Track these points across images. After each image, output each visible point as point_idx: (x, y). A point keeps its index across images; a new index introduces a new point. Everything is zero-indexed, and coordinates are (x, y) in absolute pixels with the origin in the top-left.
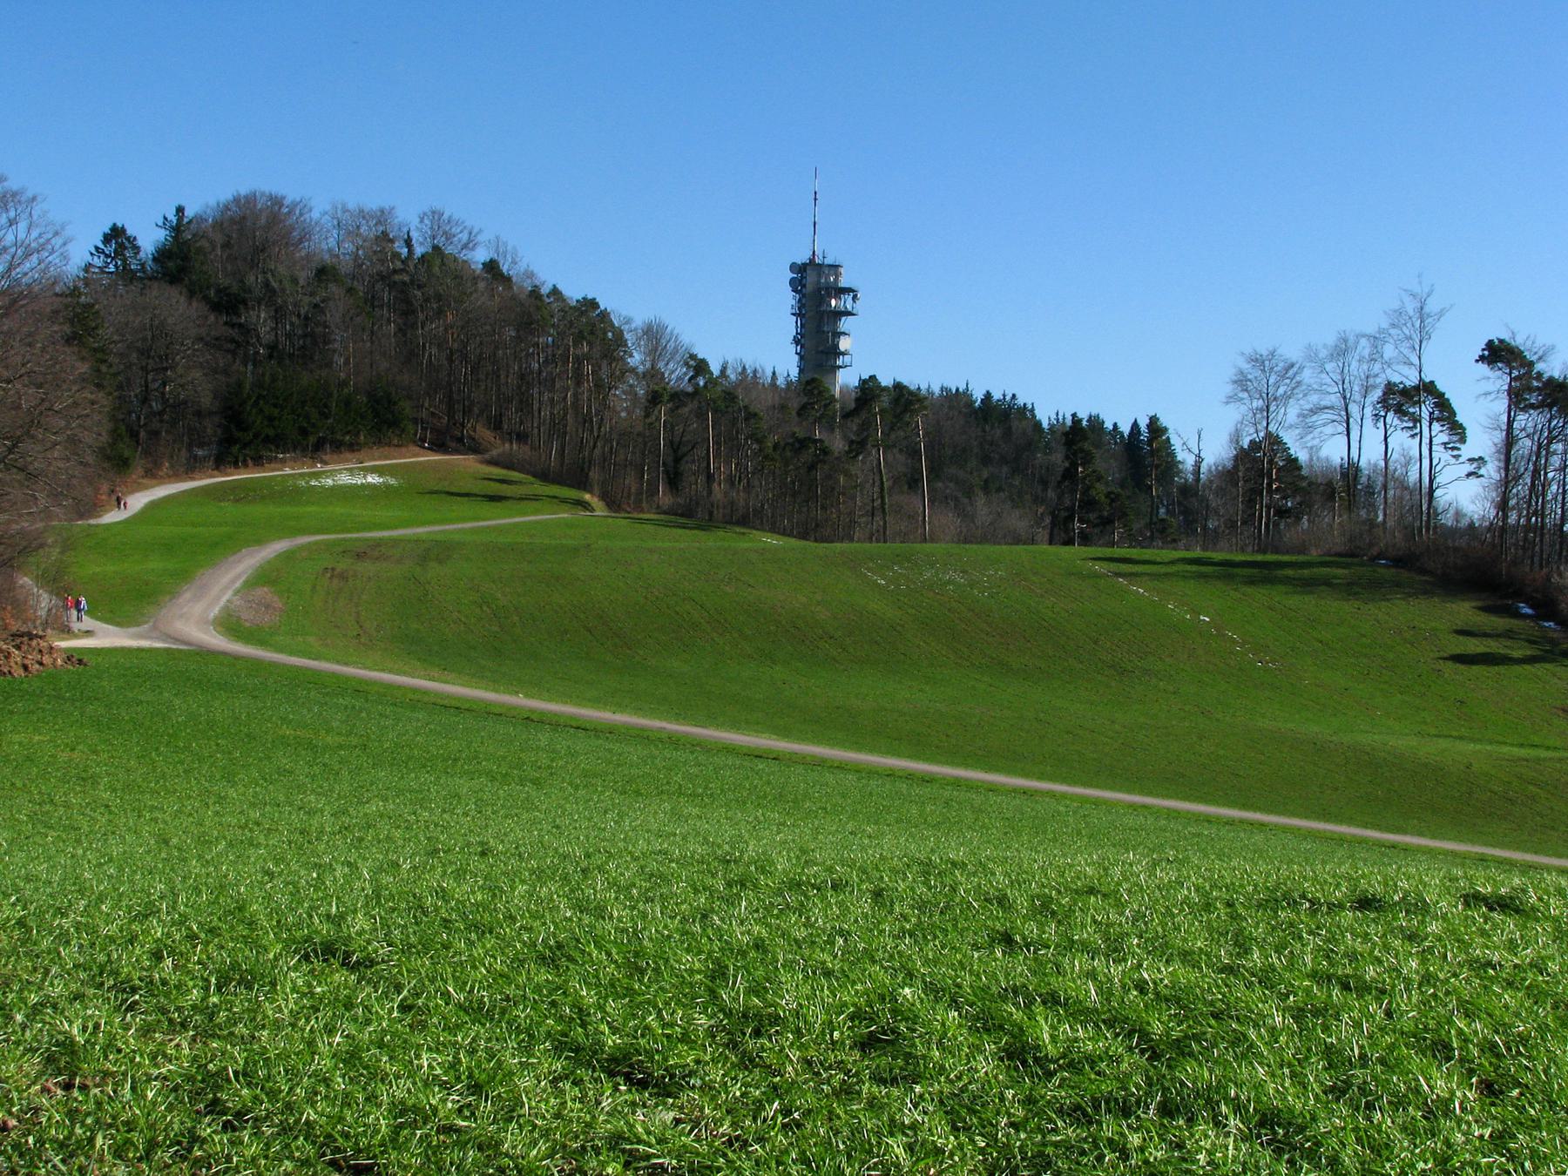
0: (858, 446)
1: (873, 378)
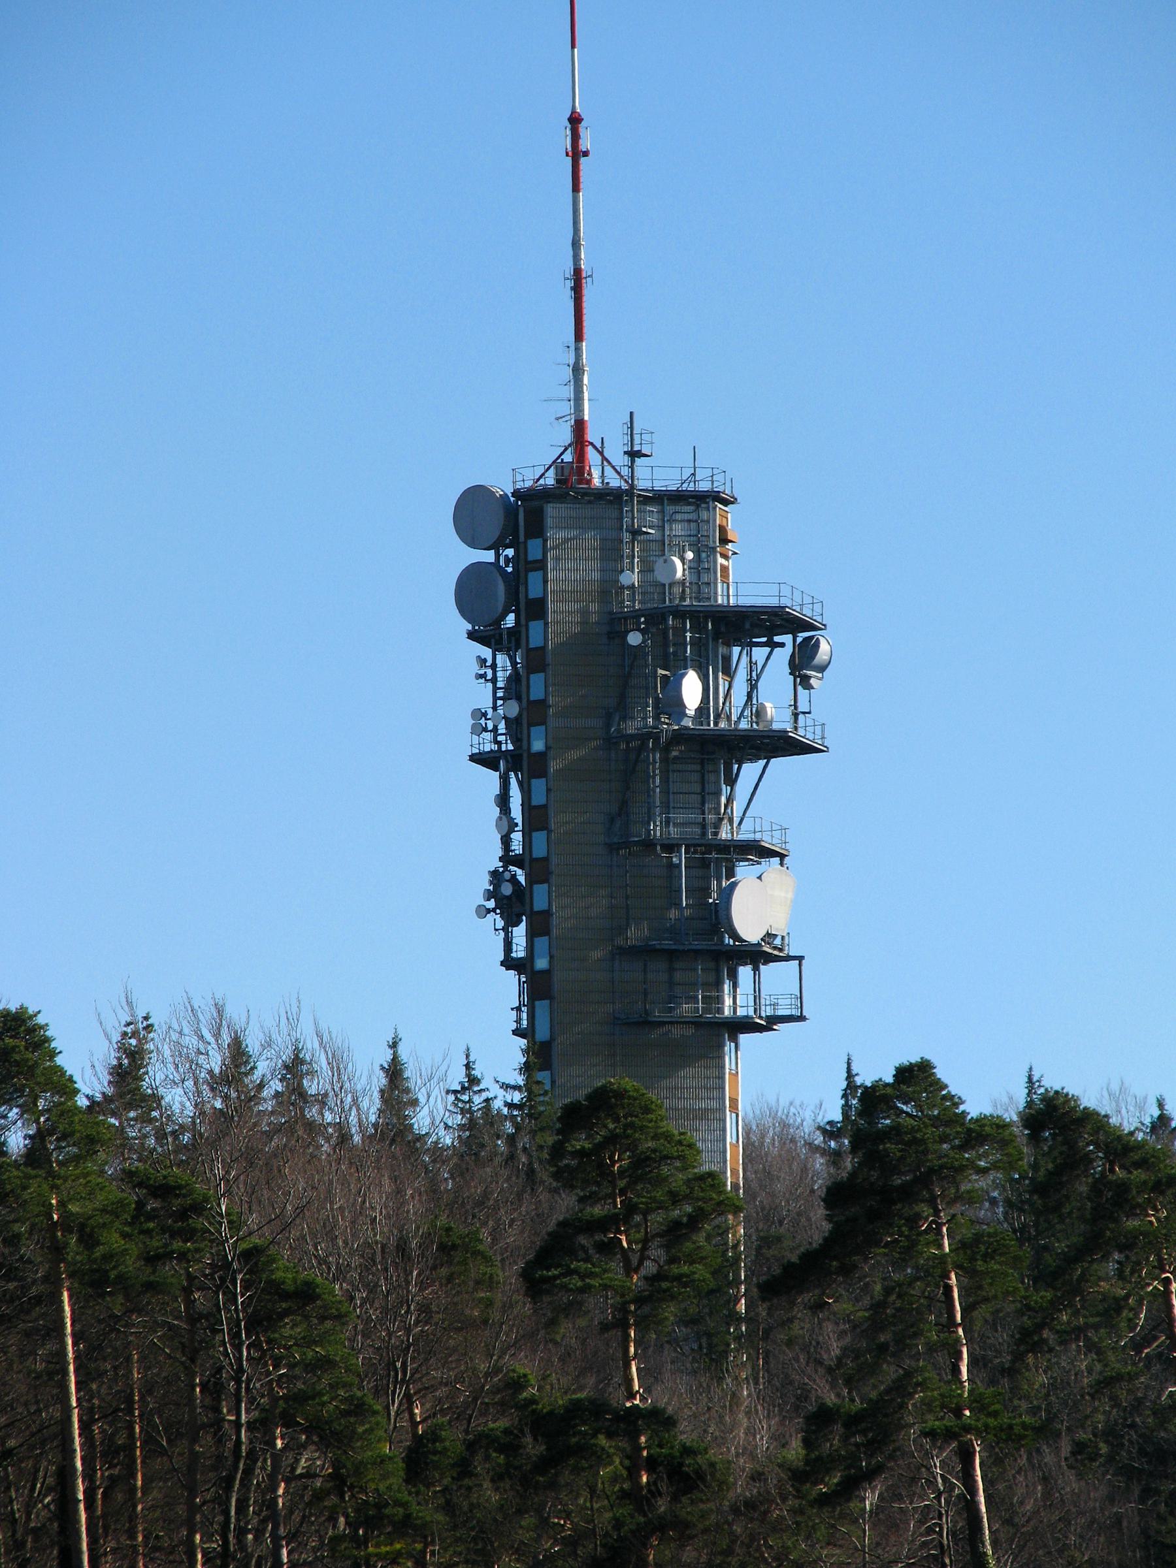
0: (849, 1445)
1: (916, 1077)
